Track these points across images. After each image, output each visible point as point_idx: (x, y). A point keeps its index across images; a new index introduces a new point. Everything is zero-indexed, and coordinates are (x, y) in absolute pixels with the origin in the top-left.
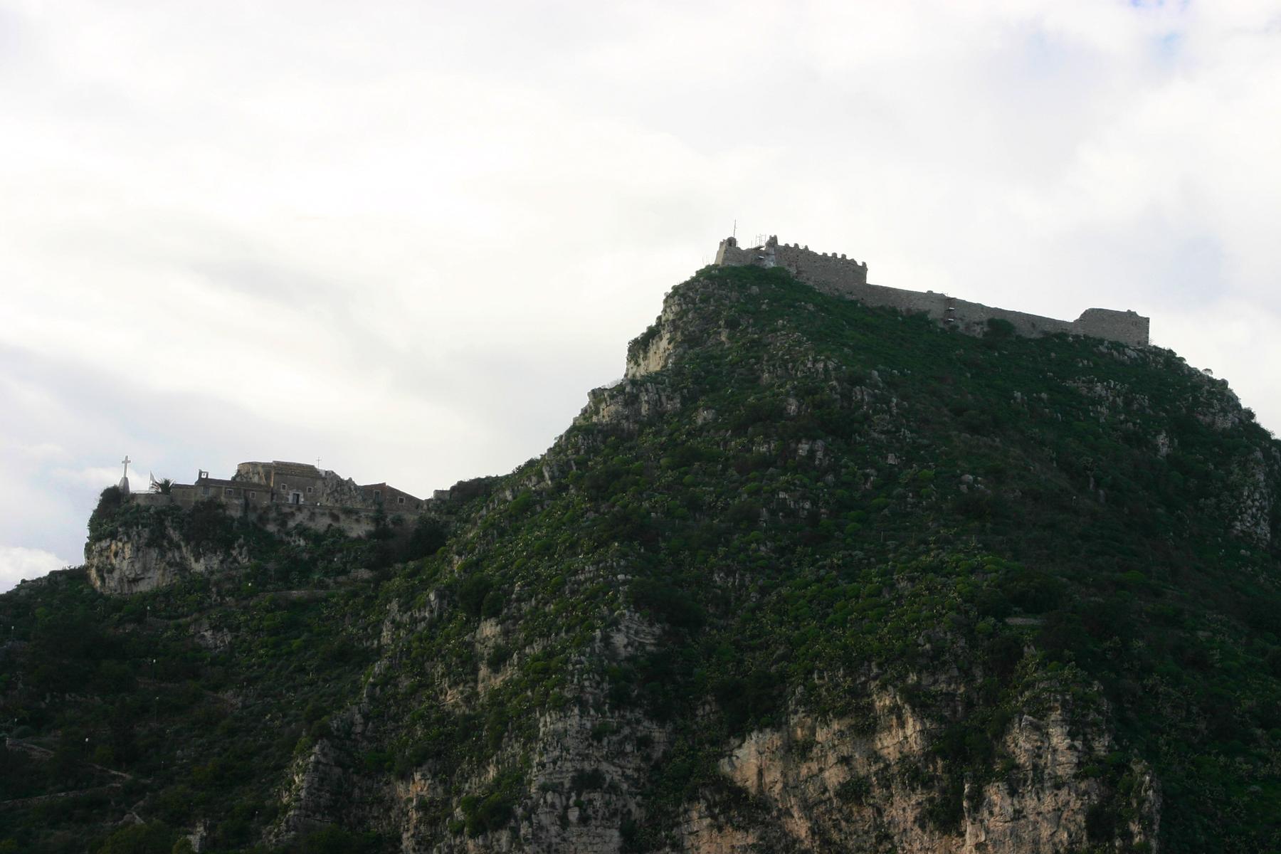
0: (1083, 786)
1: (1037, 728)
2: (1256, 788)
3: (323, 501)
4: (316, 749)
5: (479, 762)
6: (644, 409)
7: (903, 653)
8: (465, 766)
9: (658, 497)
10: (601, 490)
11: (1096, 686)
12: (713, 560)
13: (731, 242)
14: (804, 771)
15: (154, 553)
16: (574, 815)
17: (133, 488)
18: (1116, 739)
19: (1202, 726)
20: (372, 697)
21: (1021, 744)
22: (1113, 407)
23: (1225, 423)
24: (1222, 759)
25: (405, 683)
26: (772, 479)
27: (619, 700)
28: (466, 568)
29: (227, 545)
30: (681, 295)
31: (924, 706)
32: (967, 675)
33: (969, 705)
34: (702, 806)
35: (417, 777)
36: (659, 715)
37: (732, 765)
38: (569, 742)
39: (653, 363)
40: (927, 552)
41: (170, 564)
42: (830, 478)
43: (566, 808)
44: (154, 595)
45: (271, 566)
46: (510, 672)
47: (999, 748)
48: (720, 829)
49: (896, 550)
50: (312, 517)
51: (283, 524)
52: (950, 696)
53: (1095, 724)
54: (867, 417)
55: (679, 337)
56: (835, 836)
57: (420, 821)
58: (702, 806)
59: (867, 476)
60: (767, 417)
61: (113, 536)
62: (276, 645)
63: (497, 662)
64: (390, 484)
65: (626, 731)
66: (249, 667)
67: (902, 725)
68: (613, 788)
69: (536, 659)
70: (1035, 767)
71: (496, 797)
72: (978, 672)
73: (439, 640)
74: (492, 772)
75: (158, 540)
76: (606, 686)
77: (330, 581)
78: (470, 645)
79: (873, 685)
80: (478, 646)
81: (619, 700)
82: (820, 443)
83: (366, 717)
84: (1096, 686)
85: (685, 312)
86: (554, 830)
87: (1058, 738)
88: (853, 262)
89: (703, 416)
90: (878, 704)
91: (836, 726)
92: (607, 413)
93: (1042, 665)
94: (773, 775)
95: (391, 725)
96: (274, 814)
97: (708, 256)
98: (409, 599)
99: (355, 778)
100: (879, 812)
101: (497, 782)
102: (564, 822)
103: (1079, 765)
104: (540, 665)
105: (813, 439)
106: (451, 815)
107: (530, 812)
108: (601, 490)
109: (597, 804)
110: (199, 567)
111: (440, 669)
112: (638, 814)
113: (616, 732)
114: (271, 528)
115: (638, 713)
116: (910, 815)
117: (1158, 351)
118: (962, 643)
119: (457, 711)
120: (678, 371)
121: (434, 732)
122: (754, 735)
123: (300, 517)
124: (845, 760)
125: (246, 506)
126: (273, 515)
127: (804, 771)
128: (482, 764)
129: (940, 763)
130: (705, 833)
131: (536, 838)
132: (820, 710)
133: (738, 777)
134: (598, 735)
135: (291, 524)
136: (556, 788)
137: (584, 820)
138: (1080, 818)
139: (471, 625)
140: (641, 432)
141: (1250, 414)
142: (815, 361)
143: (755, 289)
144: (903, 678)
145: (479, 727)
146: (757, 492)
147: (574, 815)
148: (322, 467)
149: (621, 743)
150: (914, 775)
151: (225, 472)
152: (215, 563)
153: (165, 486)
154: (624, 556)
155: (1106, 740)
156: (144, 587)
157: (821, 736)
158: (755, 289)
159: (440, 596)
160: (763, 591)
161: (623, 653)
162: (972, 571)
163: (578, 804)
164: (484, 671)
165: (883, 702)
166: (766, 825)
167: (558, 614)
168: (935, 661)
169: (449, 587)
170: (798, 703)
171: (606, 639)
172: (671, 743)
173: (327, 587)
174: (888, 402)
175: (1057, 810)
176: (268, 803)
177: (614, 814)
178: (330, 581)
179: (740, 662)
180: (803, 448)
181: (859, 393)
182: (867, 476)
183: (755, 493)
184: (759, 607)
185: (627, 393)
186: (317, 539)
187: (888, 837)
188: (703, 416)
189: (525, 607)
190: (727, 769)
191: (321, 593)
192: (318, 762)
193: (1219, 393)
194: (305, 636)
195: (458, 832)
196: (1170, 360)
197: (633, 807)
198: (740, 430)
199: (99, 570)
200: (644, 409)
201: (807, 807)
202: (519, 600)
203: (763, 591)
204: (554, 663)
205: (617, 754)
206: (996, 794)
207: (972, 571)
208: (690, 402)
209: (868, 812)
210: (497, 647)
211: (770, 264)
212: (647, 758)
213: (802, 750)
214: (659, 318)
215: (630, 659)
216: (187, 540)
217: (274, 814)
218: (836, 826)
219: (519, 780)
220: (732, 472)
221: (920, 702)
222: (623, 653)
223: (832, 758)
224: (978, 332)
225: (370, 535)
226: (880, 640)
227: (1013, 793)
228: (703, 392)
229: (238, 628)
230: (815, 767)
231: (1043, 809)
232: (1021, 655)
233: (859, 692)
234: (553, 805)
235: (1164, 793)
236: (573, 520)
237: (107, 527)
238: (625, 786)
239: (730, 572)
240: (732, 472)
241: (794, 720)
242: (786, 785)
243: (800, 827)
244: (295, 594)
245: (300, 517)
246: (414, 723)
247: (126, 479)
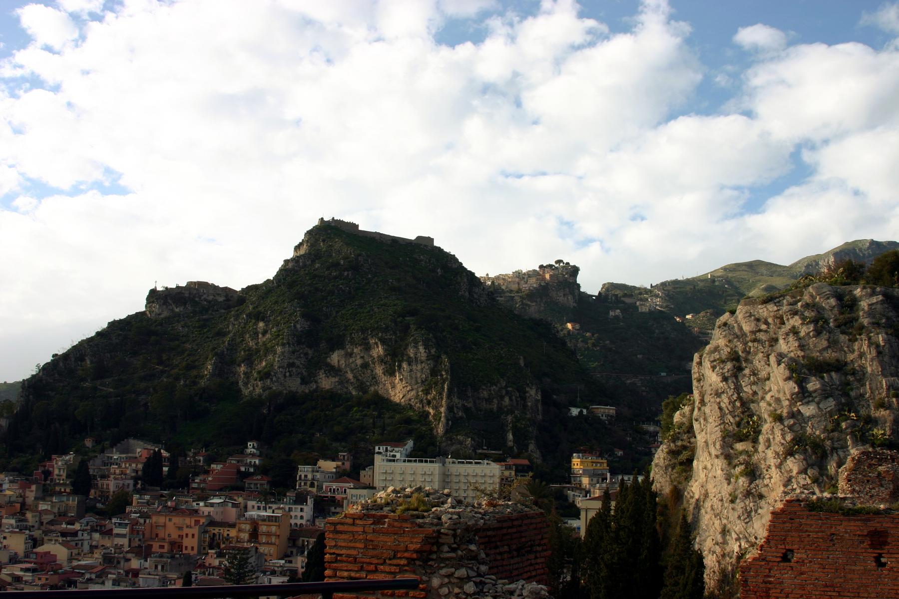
0: (429, 362)
1: (416, 347)
2: (474, 362)
3: (211, 292)
4: (214, 358)
5: (260, 361)
6: (301, 264)
7: (377, 328)
8: (256, 362)
9: (306, 288)
10: (290, 286)
11: (431, 335)
12: (323, 304)
13: (322, 219)
14: (351, 361)
15: (165, 307)
16: (288, 374)
17: (158, 289)
18: (437, 349)
19: (459, 345)
20: (229, 344)
21: (411, 352)
22: (426, 262)
23: (455, 266)
24: (465, 354)
25: (238, 340)
26: (338, 282)
27: (299, 343)
28: (254, 308)
29: (185, 304)
30: (309, 233)
31: (384, 342)
32: (395, 333)
33: (396, 341)
34: (323, 371)
35: (243, 365)
36: (310, 347)
37: (331, 359)
38: (285, 354)
39: (302, 252)
40: (382, 300)
41: (169, 310)
42: (353, 281)
43: (285, 372)
44: (165, 318)
45: (197, 309)
46: (268, 336)
47: (405, 353)
48: (328, 377)
49: (373, 300)
50: (208, 296)
51: (200, 298)
52: (391, 339)
53: (431, 345)
54: (362, 265)
55: (309, 244)
56: (360, 378)
57: (244, 377)
58: (323, 371)
59: (363, 281)
60: (336, 265)
61: (153, 302)
62: (200, 331)
63: (265, 333)
64: (229, 286)
65: (301, 351)
66: (193, 337)
67: (378, 347)
68: (298, 367)
69: (275, 332)
70: (415, 357)
71: (266, 370)
72: (398, 332)
73: (247, 328)
74: (264, 363)
75: (165, 303)
76: (295, 339)
77: (214, 313)
78: (256, 329)
79: (369, 337)
80: (258, 329)
81: (299, 343)
82: (350, 272)
83: (228, 349)
84: (431, 335)
85: (311, 238)
86: (282, 378)
87: (421, 349)
88: (355, 224)
89: (317, 265)
90: (371, 342)
91: (359, 348)
92: (290, 265)
93: (416, 330)
94: (342, 362)
95: (234, 351)
96: (202, 377)
97: (316, 223)
98: (237, 317)
99: (225, 366)
100: (372, 371)
101: (266, 366)
102: (285, 376)
103: (427, 357)
104: (276, 334)
105: (348, 271)
106: (253, 375)
107: (276, 373)
108: (290, 286)
109: (294, 371)
110: (177, 310)
111: (248, 336)
112: (305, 374)
113: (298, 351)
114: (197, 299)
115: (304, 346)
116: (381, 372)
117: (436, 247)
118: (393, 324)
119: (254, 347)
120: (310, 254)
121: (247, 353)
122: (337, 351)
123: (205, 296)
124: (362, 357)
125: (190, 293)
126: (197, 296)
127: (351, 361)
128: (261, 361)
129: (389, 357)
130: (324, 378)
131: (277, 381)
132: (353, 343)
133: (332, 363)
134: (293, 352)
135: (202, 298)
136: (282, 367)
137: (290, 375)
138: (428, 371)
139: (256, 324)
140: (300, 270)
141: (461, 264)
142: (347, 250)
143: (329, 231)
144: (377, 334)
145: (260, 351)
146: (333, 286)
147: (288, 374)
148: (210, 282)
149: (300, 354)
150: (382, 361)
151: (183, 284)
152: (182, 309)
153: (167, 288)
154: (299, 303)
155: (434, 350)
156: (162, 316)
157: (355, 350)
158: (329, 231)
159: (247, 316)
160: (337, 312)
161: (299, 330)
162: (395, 305)
163: (289, 371)
164: (260, 336)
165: (372, 341)
166: (341, 375)
167: (281, 320)
168: (386, 330)
169: (249, 313)
170: (349, 342)
171: (295, 326)
172: (313, 354)
173: (213, 315)
174: (368, 261)
175: (422, 369)
176: (201, 374)
177: (299, 374)
178: (214, 313)
179: (332, 332)
180: (346, 273)
181: (360, 258)
182: (363, 281)
183: (333, 286)
184: (336, 317)
185: (295, 260)
186: (209, 302)
187: (375, 378)
188: (317, 265)
189: (271, 318)
190: (329, 361)
191: (212, 316)
192: (214, 362)
193: (453, 258)
194: (208, 328)
195: (256, 380)
196: (439, 250)
197: (304, 372)
198: (328, 269)
199: (149, 312)
200: (301, 264)
201: (352, 371)
202: (269, 316)
203: (337, 312)
204: (281, 333)
205: (298, 358)
206: (405, 365)
207: (395, 305)
208: (313, 261)
209: (369, 371)
210: (264, 329)
211: (333, 225)
212: (307, 359)
213: (351, 355)
214: (303, 240)
215: (301, 331)
216: (174, 303)
217: (202, 377)
218: (361, 376)
219: (272, 365)
220: (326, 280)
221: (383, 341)
222: (299, 330)
223: (358, 357)
224: (389, 242)
225: (224, 301)
226: (371, 324)
227: (409, 365)
228: (317, 259)
229: (189, 327)
230: (354, 359)
231: (418, 369)
232: (410, 327)
233: (365, 339)
234: (282, 372)
235: (450, 363)
236: (283, 294)
237: (152, 300)
238: (301, 366)
239: (327, 307)
240: (326, 280)
241: (347, 347)
242: (346, 365)
243: (350, 376)
244: (204, 317)
245: (205, 296)
246: (241, 351)
247: (156, 287)
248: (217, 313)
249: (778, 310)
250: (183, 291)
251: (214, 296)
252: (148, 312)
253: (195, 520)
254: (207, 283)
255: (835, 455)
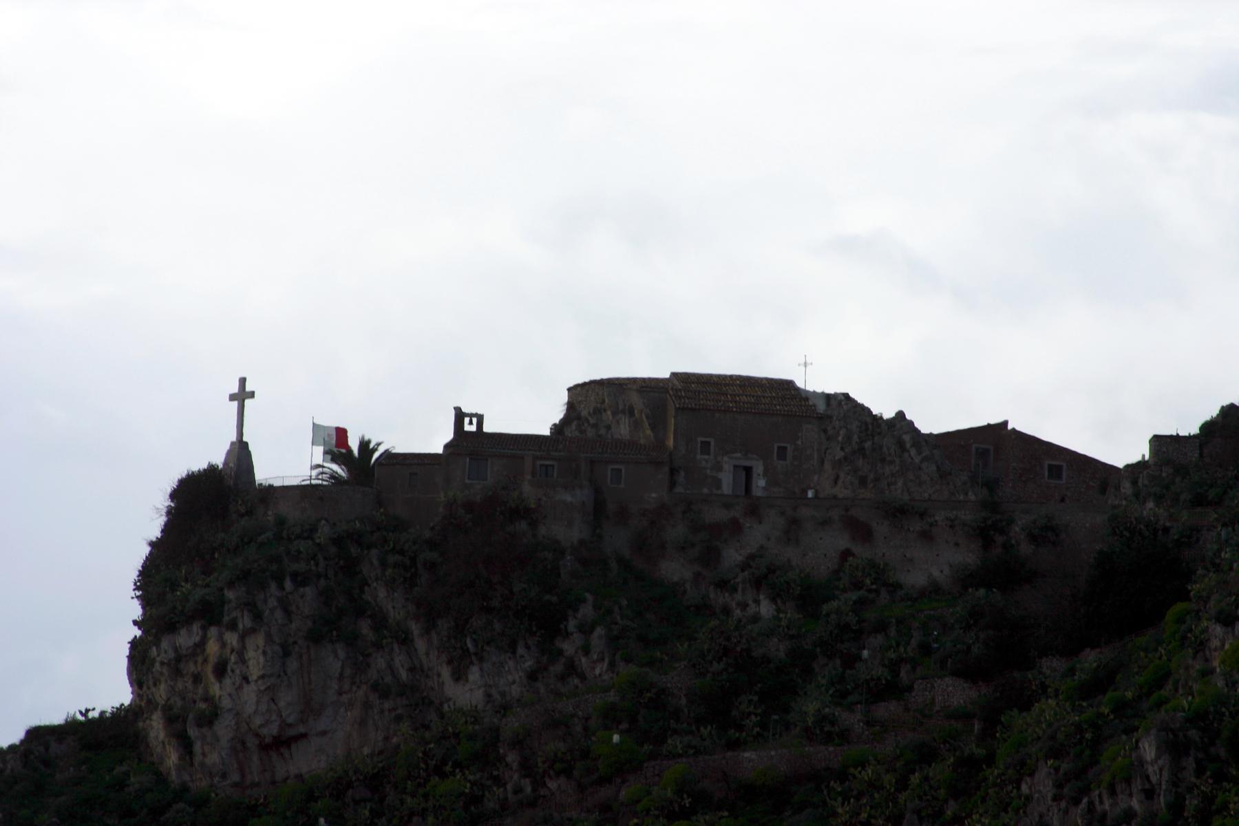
15: (333, 659)
51: (710, 557)
61: (209, 613)
77: (853, 719)
114: (674, 570)
125: (598, 511)
126: (676, 531)
135: (732, 556)
159: (1175, 748)
169: (1198, 718)
173: (844, 736)
178: (853, 719)
191: (824, 755)
199: (174, 720)
225: (968, 580)
247: (241, 451)
248: (886, 710)
249: (1072, 671)
250: (529, 491)
251: (861, 532)
252: (156, 728)
253: (486, 480)
254: (787, 386)
255: (196, 627)
